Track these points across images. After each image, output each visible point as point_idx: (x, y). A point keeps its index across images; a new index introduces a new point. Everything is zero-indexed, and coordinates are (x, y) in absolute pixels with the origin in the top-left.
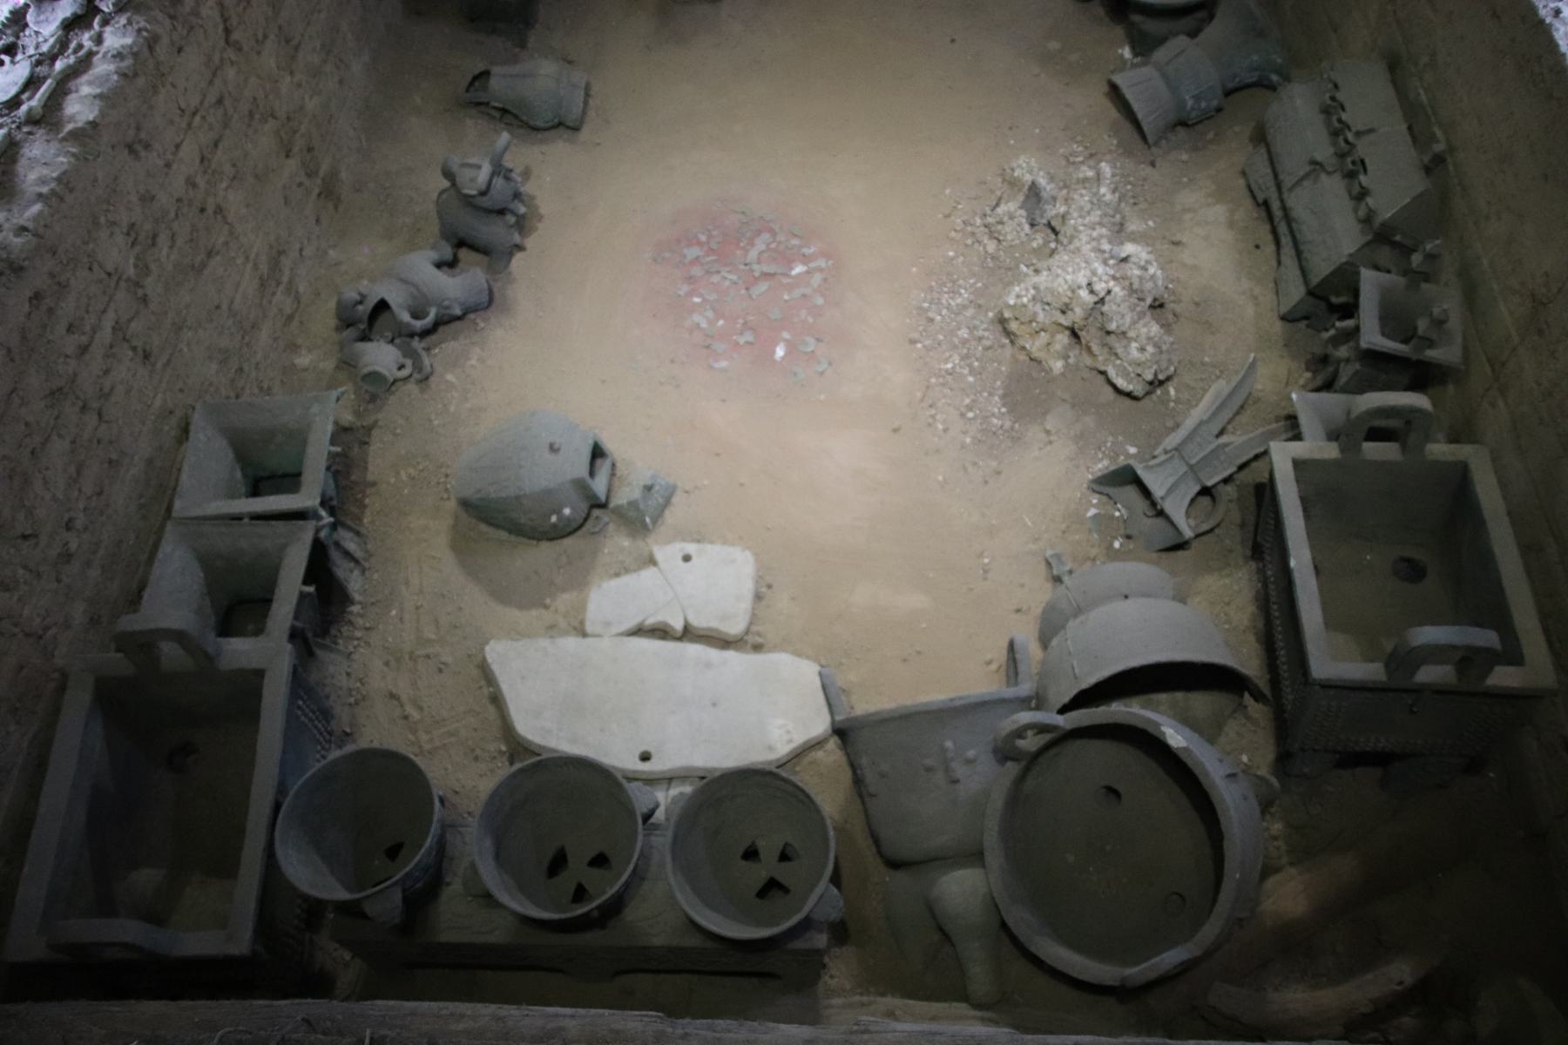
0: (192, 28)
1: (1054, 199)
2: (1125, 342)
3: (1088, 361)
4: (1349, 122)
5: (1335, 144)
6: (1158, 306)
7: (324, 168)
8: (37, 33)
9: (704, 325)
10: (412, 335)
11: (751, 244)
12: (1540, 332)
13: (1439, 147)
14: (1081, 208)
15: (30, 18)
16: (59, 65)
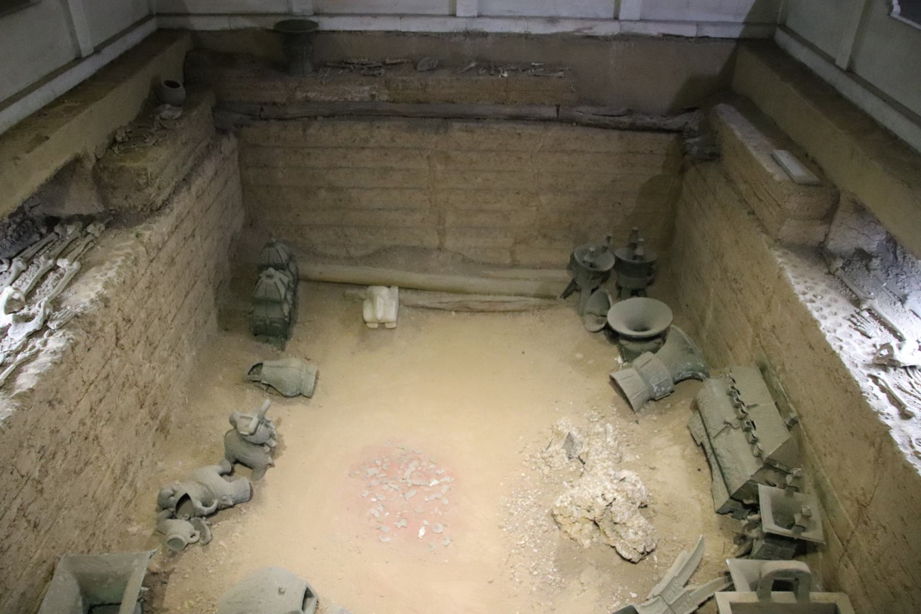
0: (98, 338)
1: (582, 443)
2: (625, 529)
3: (605, 540)
4: (743, 400)
5: (737, 412)
6: (644, 506)
7: (162, 414)
8: (12, 339)
9: (377, 515)
10: (201, 516)
11: (407, 466)
12: (866, 523)
13: (793, 415)
14: (597, 450)
15: (10, 331)
16: (20, 357)
